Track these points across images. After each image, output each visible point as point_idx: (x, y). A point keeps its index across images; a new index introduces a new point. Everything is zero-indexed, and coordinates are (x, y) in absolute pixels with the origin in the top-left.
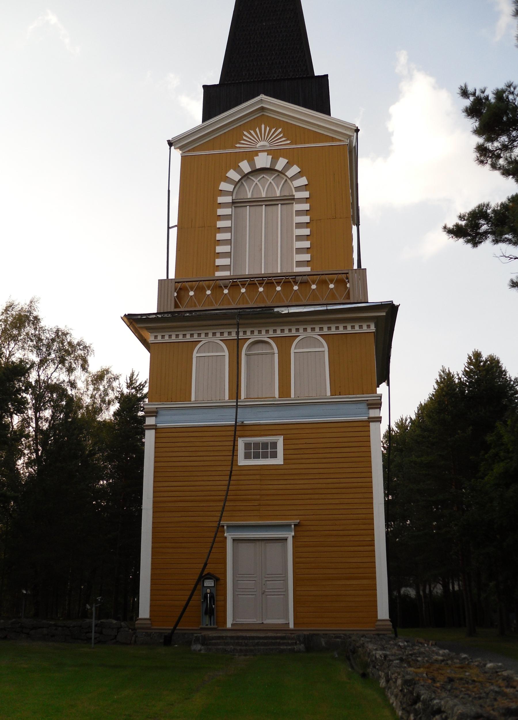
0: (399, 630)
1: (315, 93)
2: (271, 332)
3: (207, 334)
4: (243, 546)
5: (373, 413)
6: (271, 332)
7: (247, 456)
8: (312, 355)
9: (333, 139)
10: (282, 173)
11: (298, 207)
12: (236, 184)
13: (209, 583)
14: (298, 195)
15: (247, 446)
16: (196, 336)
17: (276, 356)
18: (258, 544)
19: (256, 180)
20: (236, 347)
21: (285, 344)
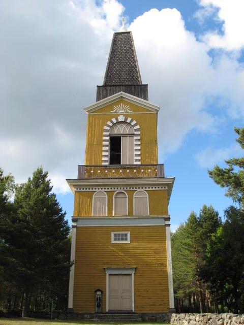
0: (200, 37)
1: (141, 90)
2: (125, 189)
3: (98, 189)
4: (113, 278)
5: (167, 223)
6: (125, 189)
7: (115, 239)
8: (142, 198)
9: (150, 111)
10: (129, 124)
11: (135, 138)
12: (110, 127)
13: (99, 293)
14: (136, 133)
15: (115, 235)
16: (94, 189)
17: (127, 198)
18: (120, 277)
19: (119, 126)
20: (110, 194)
21: (131, 193)
